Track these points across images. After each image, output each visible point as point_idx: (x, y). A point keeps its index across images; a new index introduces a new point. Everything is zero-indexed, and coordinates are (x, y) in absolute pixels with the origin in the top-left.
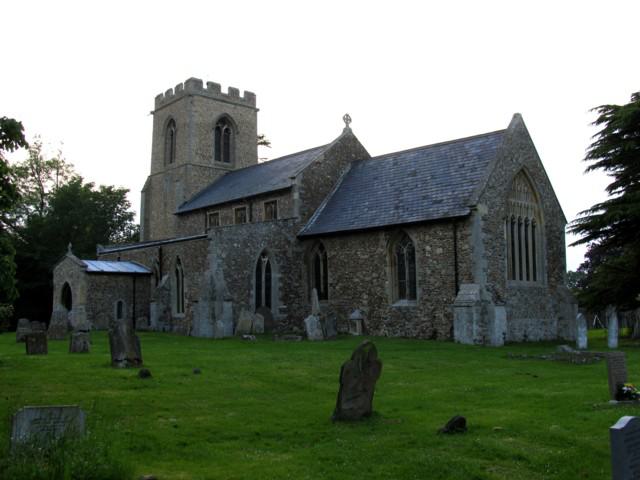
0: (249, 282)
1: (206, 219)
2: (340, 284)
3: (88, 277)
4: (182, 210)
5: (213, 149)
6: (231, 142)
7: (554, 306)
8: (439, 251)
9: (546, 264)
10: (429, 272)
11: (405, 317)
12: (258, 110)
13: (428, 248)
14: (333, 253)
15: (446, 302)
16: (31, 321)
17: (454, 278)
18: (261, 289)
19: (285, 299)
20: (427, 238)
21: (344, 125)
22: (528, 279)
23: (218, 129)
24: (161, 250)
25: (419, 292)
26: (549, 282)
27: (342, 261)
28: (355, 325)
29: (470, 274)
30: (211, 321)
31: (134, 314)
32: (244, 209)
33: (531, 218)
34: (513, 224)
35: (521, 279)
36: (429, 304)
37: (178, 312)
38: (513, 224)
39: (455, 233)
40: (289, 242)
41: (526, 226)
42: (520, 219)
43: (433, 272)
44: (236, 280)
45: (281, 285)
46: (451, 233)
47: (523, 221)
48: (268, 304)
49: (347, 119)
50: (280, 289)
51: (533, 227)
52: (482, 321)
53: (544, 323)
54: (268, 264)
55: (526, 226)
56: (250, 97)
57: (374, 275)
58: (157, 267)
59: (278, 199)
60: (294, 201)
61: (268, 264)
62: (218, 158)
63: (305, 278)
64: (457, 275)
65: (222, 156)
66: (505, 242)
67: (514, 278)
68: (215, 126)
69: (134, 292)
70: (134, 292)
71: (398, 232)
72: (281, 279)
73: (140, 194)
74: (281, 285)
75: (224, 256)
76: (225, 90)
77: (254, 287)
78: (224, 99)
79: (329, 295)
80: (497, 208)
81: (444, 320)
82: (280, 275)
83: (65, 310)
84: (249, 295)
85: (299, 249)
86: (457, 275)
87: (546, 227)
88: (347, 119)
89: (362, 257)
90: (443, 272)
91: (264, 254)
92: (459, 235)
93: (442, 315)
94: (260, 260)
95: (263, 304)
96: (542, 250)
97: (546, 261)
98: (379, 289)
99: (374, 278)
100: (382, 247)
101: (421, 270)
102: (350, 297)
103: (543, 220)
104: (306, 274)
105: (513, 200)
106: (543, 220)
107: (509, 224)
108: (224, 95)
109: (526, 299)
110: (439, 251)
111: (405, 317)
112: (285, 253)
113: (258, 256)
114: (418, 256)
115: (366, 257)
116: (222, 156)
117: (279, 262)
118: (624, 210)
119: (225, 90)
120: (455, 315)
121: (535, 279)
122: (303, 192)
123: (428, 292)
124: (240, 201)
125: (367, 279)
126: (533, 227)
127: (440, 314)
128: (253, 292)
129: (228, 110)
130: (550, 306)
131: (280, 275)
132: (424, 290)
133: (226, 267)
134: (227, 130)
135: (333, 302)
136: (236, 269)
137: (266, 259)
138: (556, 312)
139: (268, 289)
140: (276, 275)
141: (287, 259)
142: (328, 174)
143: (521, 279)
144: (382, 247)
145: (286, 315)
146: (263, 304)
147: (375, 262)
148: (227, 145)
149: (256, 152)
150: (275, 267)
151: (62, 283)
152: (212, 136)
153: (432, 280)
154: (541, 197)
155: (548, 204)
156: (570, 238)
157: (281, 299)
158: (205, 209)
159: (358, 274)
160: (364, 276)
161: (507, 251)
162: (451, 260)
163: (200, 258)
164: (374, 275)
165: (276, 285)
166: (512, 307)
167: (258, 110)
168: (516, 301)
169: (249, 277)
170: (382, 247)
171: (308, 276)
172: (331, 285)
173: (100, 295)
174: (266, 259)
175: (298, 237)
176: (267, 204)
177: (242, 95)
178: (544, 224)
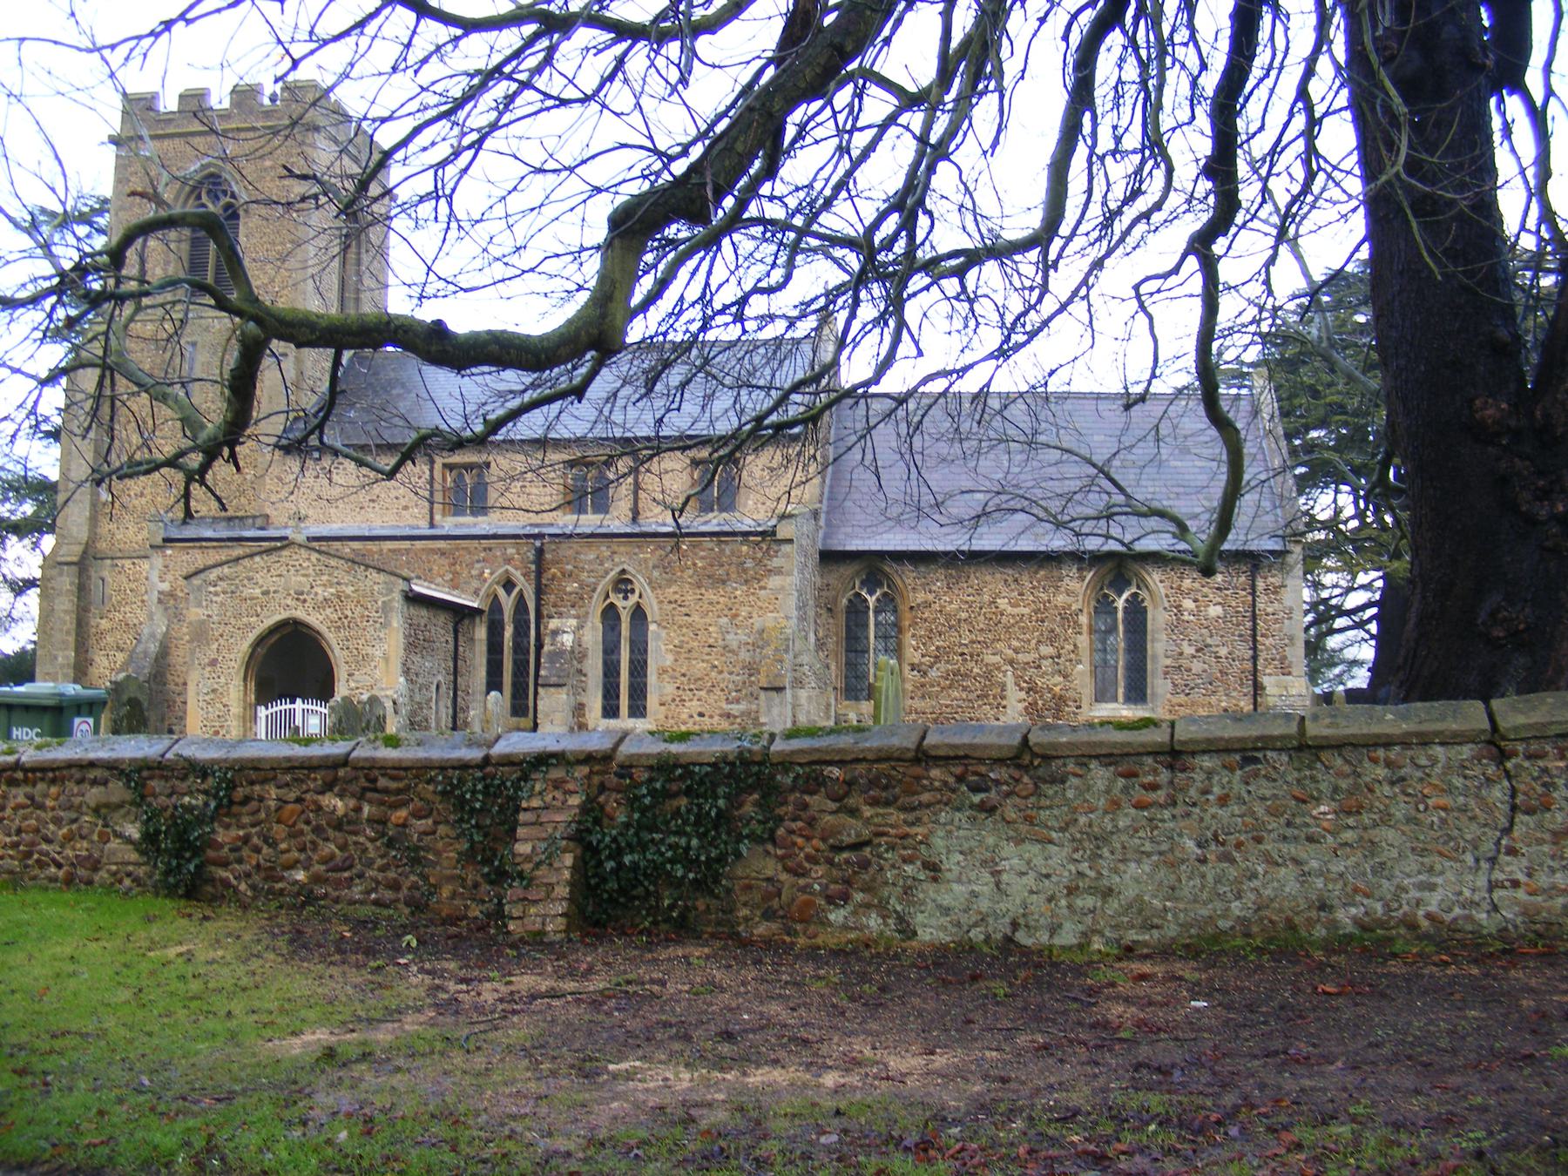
8: (1215, 611)
10: (1189, 650)
13: (1188, 604)
14: (921, 597)
16: (1543, 344)
17: (1249, 665)
18: (631, 686)
20: (1187, 583)
27: (948, 617)
37: (611, 711)
57: (1046, 650)
61: (639, 614)
73: (720, 33)
76: (220, 100)
83: (178, 657)
86: (1255, 658)
89: (1010, 610)
92: (1260, 585)
102: (972, 696)
118: (569, 677)
125: (1028, 658)
144: (1075, 589)
153: (1197, 666)
160: (1016, 651)
170: (1075, 589)
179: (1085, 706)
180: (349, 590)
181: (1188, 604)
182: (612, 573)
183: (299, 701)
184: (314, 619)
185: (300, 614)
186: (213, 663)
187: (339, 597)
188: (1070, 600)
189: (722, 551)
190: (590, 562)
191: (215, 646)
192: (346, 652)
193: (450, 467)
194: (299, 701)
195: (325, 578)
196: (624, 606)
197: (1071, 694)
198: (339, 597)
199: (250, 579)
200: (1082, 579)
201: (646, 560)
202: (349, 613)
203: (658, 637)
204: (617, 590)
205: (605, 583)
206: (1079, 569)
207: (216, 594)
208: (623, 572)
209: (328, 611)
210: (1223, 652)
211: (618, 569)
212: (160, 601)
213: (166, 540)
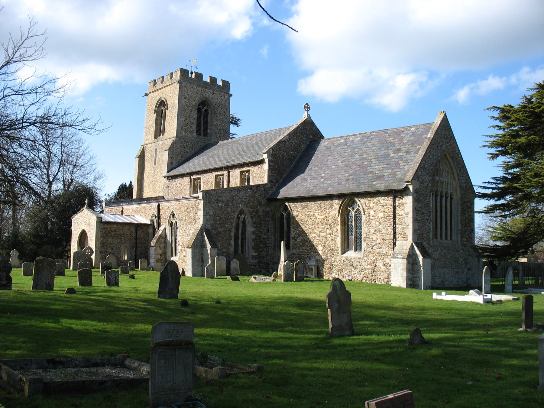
0: (230, 235)
1: (191, 181)
2: (301, 238)
3: (102, 226)
4: (170, 174)
5: (195, 126)
6: (209, 120)
7: (464, 260)
9: (460, 228)
10: (372, 231)
11: (352, 265)
12: (231, 95)
15: (384, 255)
19: (256, 248)
22: (446, 239)
23: (199, 111)
24: (159, 206)
25: (364, 245)
26: (462, 240)
28: (312, 270)
29: (405, 233)
30: (201, 264)
31: (136, 256)
32: (223, 175)
33: (449, 192)
34: (437, 196)
35: (441, 238)
36: (371, 255)
38: (437, 196)
40: (260, 203)
41: (446, 198)
42: (446, 194)
43: (375, 231)
44: (220, 232)
45: (254, 237)
47: (449, 195)
50: (253, 240)
51: (451, 199)
52: (413, 270)
53: (458, 273)
55: (446, 198)
56: (226, 84)
58: (155, 220)
59: (251, 168)
62: (198, 133)
63: (272, 231)
65: (202, 132)
66: (431, 210)
67: (436, 238)
68: (197, 108)
69: (136, 239)
70: (136, 239)
71: (348, 199)
72: (253, 232)
74: (254, 237)
75: (211, 213)
77: (233, 239)
79: (291, 245)
80: (426, 184)
81: (383, 268)
82: (253, 229)
84: (229, 244)
85: (268, 209)
87: (461, 198)
88: (307, 107)
90: (383, 231)
91: (242, 212)
93: (381, 265)
94: (238, 217)
95: (240, 252)
96: (457, 209)
97: (460, 225)
99: (328, 234)
100: (335, 209)
101: (366, 229)
103: (458, 194)
104: (273, 229)
105: (437, 178)
106: (458, 194)
107: (434, 195)
108: (206, 83)
109: (445, 254)
110: (381, 215)
111: (352, 265)
112: (257, 212)
113: (237, 213)
114: (364, 218)
115: (323, 217)
116: (202, 132)
117: (252, 219)
120: (392, 265)
121: (451, 239)
122: (272, 164)
124: (220, 169)
125: (322, 234)
126: (451, 199)
127: (380, 264)
128: (232, 242)
129: (208, 94)
130: (462, 259)
131: (253, 229)
132: (368, 245)
133: (213, 222)
134: (206, 111)
135: (294, 252)
136: (220, 224)
137: (243, 217)
138: (466, 264)
139: (244, 239)
140: (250, 229)
141: (259, 217)
142: (292, 150)
143: (441, 238)
145: (257, 261)
146: (240, 252)
147: (330, 221)
148: (206, 122)
149: (473, 204)
150: (249, 222)
151: (80, 231)
152: (195, 115)
153: (374, 237)
154: (458, 175)
155: (463, 181)
156: (480, 204)
157: (253, 248)
158: (190, 174)
159: (316, 231)
161: (432, 217)
163: (192, 214)
164: (328, 232)
165: (250, 236)
166: (434, 259)
167: (231, 95)
168: (438, 255)
169: (230, 230)
171: (275, 230)
172: (293, 238)
173: (110, 240)
174: (243, 217)
175: (267, 199)
176: (241, 173)
177: (220, 83)
178: (459, 197)
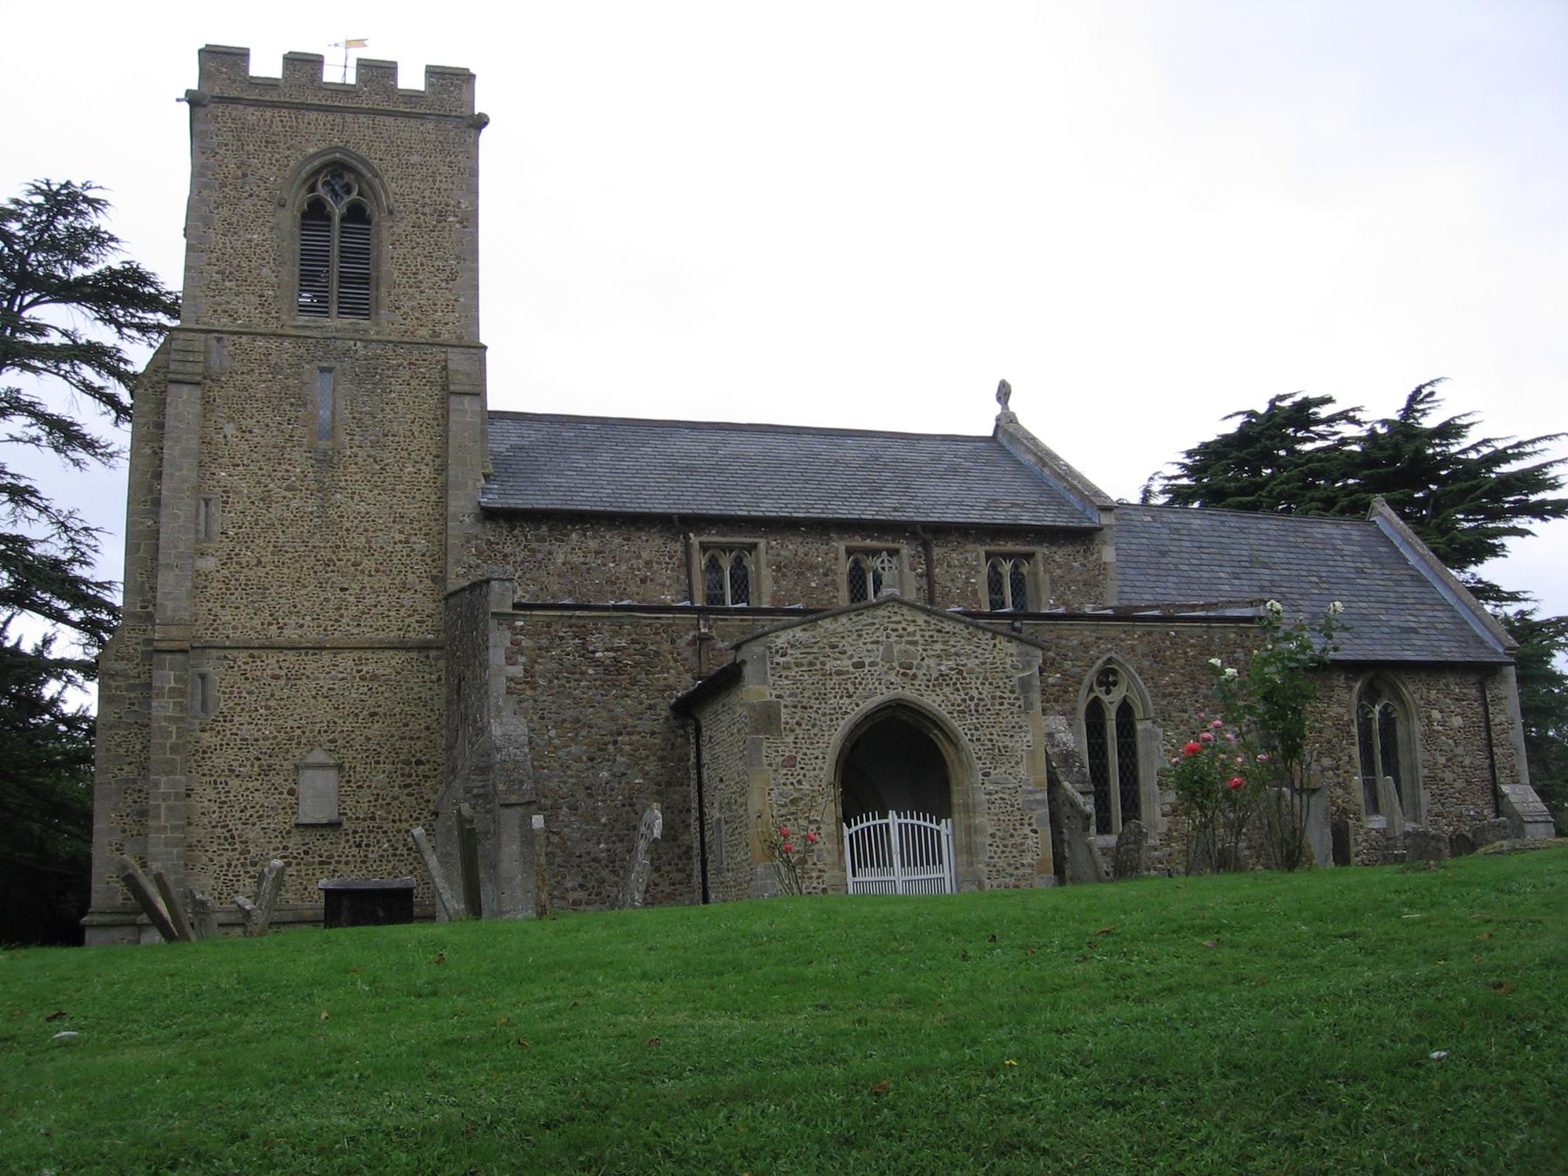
8: (1457, 721)
10: (1442, 760)
13: (1436, 714)
17: (1487, 775)
18: (1106, 781)
21: (997, 409)
39: (1483, 692)
46: (1473, 692)
48: (1132, 806)
49: (1004, 393)
54: (1125, 711)
59: (1041, 551)
60: (1103, 567)
61: (1125, 711)
64: (1492, 767)
76: (411, 79)
78: (339, 100)
91: (1107, 678)
98: (1340, 791)
101: (1427, 756)
110: (1457, 721)
119: (411, 79)
123: (1439, 798)
153: (1448, 776)
162: (1479, 742)
164: (1327, 762)
179: (1364, 818)
180: (972, 663)
181: (1436, 714)
182: (1100, 662)
183: (892, 814)
184: (932, 701)
185: (909, 694)
186: (790, 762)
187: (960, 672)
188: (1342, 711)
189: (1211, 638)
190: (1074, 648)
191: (791, 739)
192: (977, 746)
193: (705, 547)
194: (892, 814)
195: (938, 646)
196: (1111, 702)
197: (1351, 807)
198: (960, 672)
199: (833, 647)
200: (1350, 689)
201: (1133, 648)
202: (975, 693)
203: (1151, 736)
204: (1100, 684)
205: (1091, 676)
206: (1347, 679)
207: (787, 667)
208: (1110, 660)
209: (947, 690)
210: (1467, 762)
211: (1105, 658)
212: (509, 692)
213: (516, 606)
